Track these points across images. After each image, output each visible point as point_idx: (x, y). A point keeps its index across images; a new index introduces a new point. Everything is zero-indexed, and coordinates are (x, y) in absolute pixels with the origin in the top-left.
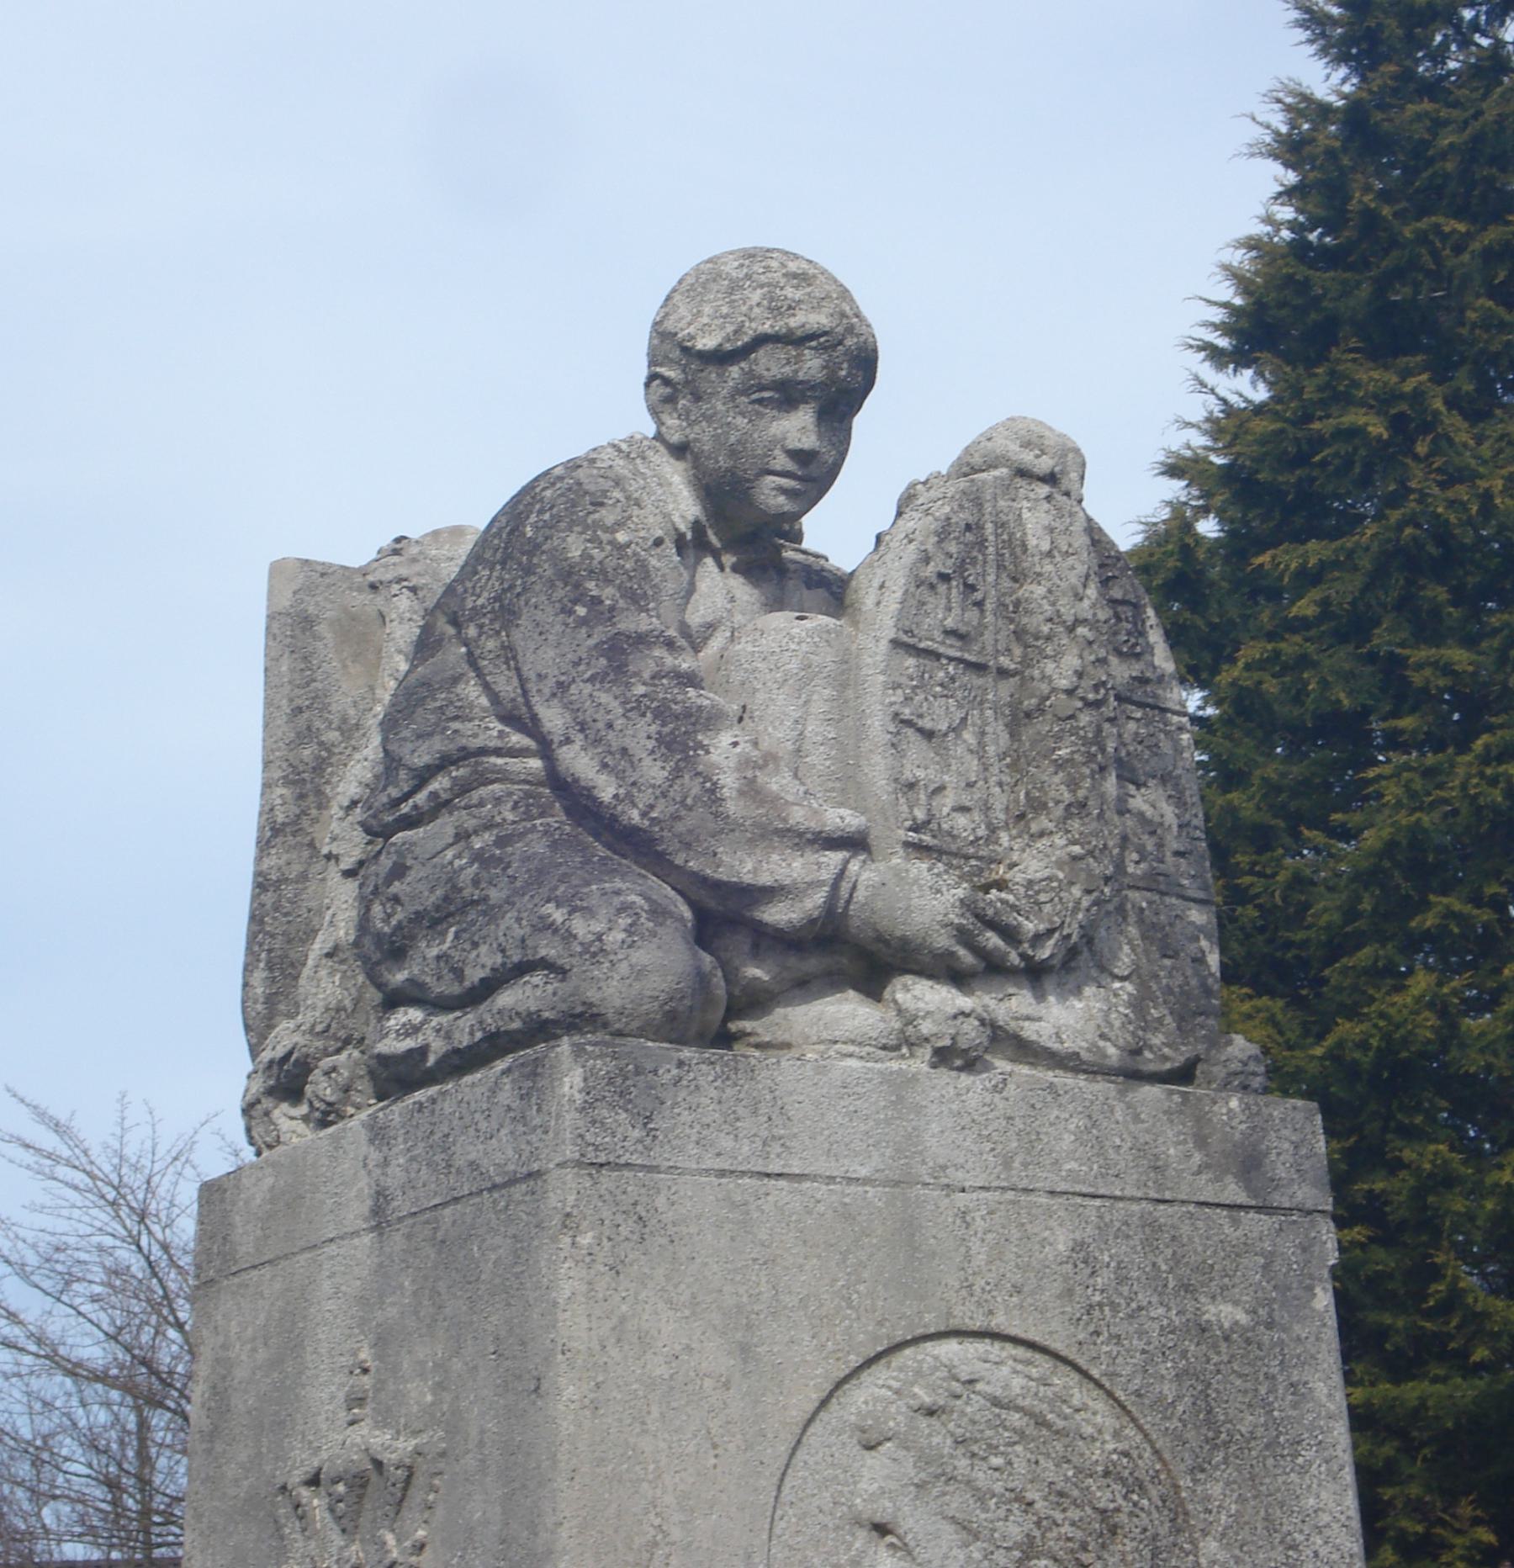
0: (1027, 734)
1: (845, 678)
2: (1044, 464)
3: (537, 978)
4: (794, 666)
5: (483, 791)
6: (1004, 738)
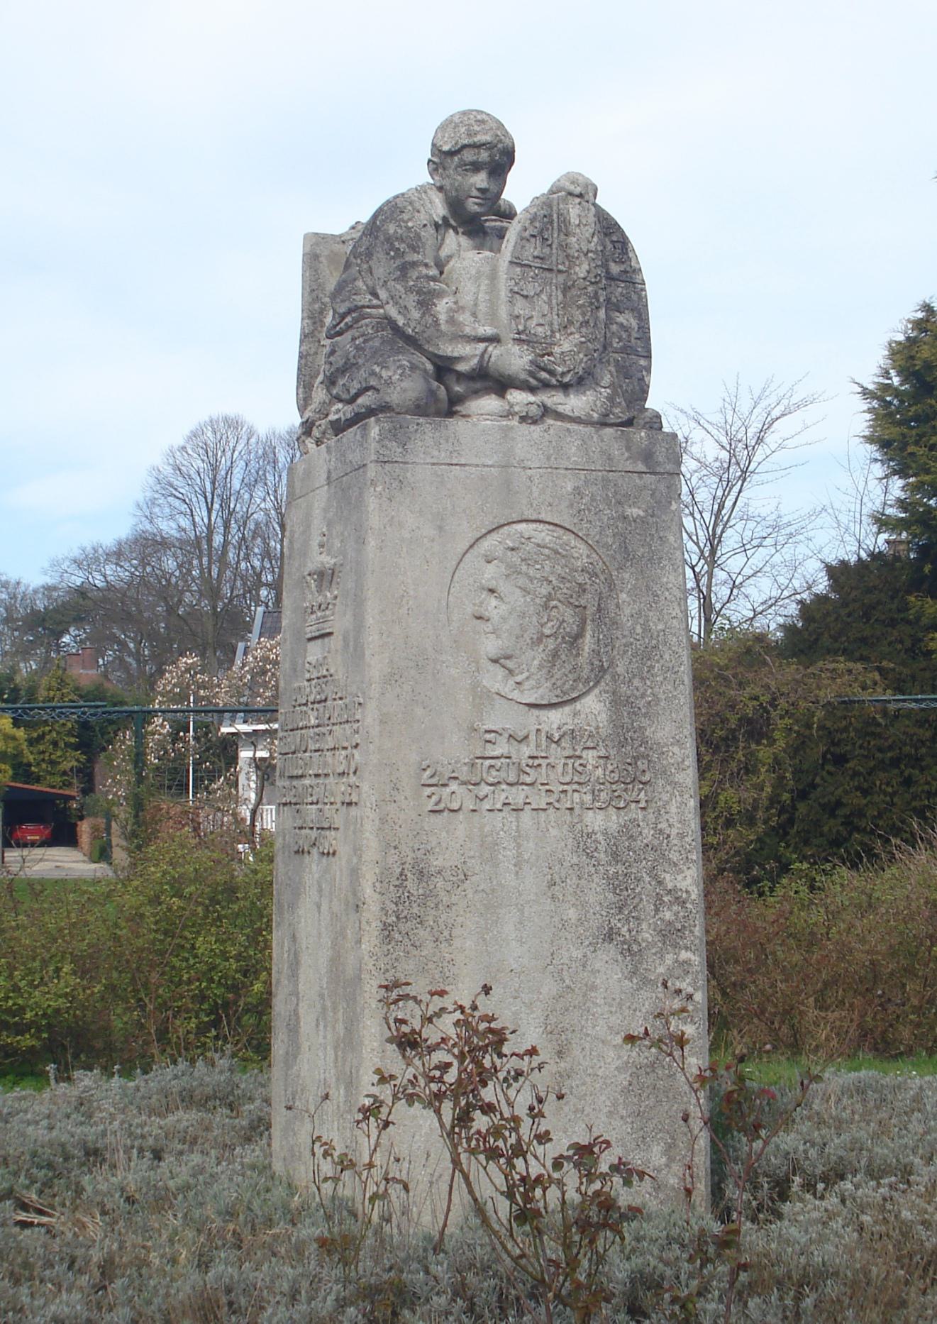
0: (569, 295)
1: (493, 276)
2: (578, 190)
3: (369, 393)
4: (473, 272)
5: (363, 322)
6: (561, 297)
